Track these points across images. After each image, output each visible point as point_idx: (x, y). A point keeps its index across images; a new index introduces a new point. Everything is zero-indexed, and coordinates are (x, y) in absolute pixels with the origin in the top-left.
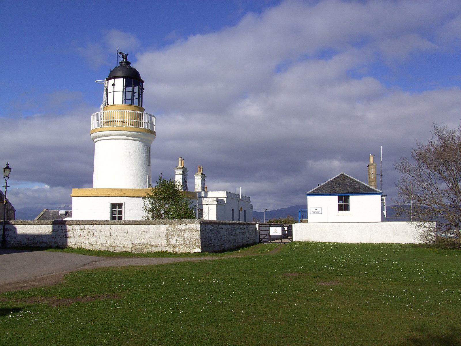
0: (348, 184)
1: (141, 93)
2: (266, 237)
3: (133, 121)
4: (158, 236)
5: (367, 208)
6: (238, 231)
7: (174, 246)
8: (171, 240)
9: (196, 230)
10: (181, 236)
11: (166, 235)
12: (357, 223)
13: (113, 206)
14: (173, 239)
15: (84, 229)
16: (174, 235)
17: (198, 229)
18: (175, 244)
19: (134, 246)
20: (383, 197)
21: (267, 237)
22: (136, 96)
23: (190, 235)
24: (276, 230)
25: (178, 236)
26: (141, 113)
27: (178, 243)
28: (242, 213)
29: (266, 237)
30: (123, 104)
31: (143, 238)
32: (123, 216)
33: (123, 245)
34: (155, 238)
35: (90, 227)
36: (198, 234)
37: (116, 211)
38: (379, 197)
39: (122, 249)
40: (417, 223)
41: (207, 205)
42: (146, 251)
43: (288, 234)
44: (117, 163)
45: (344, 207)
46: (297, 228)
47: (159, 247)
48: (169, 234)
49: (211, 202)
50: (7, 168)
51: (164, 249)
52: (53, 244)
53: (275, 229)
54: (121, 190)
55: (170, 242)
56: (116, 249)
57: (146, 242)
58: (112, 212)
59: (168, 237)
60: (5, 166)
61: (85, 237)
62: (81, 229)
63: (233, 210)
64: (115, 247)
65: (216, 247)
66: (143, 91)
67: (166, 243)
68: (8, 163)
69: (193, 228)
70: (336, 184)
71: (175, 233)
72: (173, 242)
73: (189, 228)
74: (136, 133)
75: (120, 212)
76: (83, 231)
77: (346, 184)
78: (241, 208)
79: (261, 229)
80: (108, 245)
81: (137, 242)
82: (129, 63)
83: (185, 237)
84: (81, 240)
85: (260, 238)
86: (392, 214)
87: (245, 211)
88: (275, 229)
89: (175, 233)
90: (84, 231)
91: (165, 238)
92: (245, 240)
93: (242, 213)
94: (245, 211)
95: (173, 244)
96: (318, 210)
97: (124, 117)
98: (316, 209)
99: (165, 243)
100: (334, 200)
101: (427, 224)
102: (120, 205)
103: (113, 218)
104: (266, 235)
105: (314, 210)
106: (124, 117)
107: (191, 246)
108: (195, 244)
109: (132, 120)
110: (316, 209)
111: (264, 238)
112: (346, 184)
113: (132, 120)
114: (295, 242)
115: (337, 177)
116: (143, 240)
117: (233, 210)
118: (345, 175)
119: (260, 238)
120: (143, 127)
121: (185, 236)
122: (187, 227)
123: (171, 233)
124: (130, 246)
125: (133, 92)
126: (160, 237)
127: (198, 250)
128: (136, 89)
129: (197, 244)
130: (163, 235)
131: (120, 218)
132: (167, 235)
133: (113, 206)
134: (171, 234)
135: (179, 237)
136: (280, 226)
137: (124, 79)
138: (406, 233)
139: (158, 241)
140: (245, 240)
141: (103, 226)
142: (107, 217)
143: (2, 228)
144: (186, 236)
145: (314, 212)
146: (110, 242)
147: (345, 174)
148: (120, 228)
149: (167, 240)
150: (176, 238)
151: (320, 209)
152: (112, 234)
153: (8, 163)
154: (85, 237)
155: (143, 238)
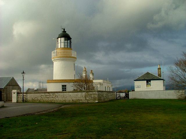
1: (70, 42)
6: (109, 94)
7: (88, 100)
12: (156, 90)
13: (63, 86)
20: (164, 81)
22: (69, 44)
28: (109, 88)
32: (67, 90)
35: (56, 94)
37: (64, 88)
38: (54, 79)
42: (78, 102)
43: (127, 95)
46: (130, 93)
51: (84, 101)
52: (106, 100)
54: (62, 80)
56: (66, 102)
58: (63, 88)
72: (87, 98)
75: (65, 88)
79: (117, 94)
81: (74, 99)
84: (52, 99)
86: (168, 87)
93: (109, 88)
99: (84, 99)
101: (181, 91)
102: (65, 86)
103: (63, 90)
111: (118, 97)
119: (116, 97)
121: (92, 96)
124: (71, 100)
128: (69, 41)
131: (65, 90)
133: (63, 86)
136: (29, 97)
138: (172, 95)
139: (82, 98)
141: (61, 93)
142: (61, 90)
143: (22, 95)
146: (64, 99)
149: (85, 98)
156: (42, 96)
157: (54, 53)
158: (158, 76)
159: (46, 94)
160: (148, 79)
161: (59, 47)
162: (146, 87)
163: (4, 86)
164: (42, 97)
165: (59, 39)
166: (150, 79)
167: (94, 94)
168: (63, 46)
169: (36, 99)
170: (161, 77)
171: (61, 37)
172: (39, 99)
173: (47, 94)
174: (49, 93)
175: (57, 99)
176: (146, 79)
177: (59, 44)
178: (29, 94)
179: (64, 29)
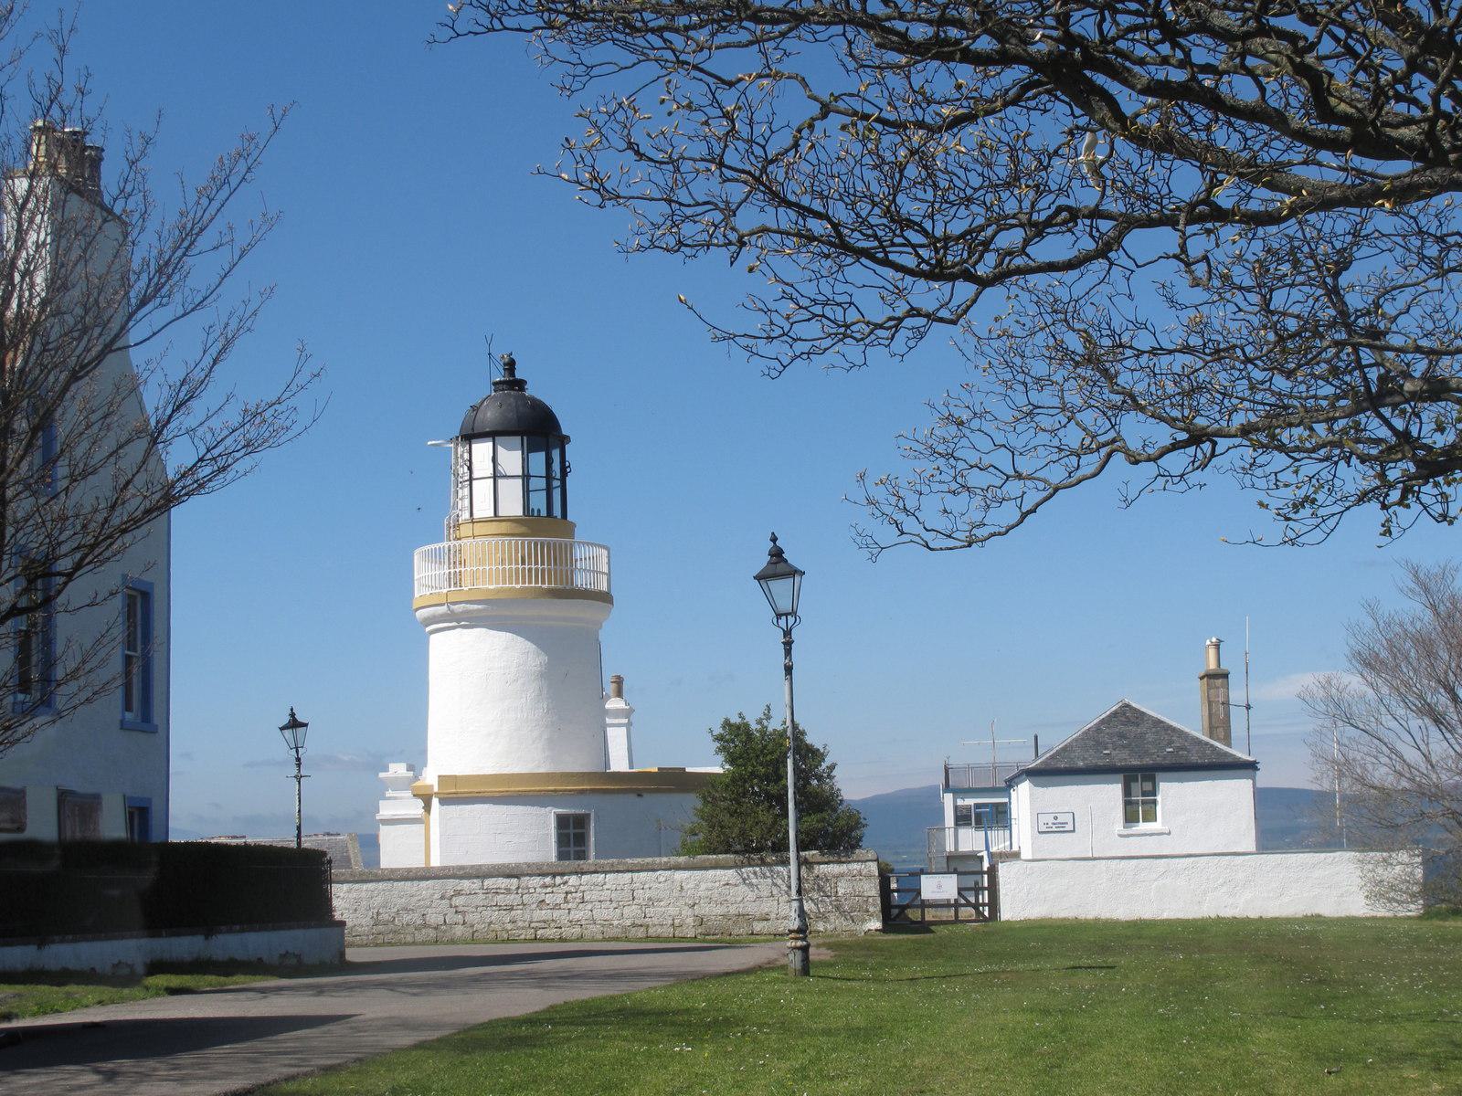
0: (1150, 737)
3: (517, 569)
5: (1204, 813)
9: (869, 876)
12: (1198, 861)
15: (555, 885)
19: (701, 921)
26: (523, 543)
33: (670, 922)
39: (668, 932)
40: (1378, 855)
44: (476, 702)
45: (1137, 809)
50: (294, 724)
54: (583, 774)
58: (562, 840)
60: (286, 720)
61: (557, 907)
62: (545, 886)
64: (648, 926)
68: (292, 710)
70: (1111, 736)
74: (476, 607)
76: (549, 890)
77: (1142, 736)
80: (628, 923)
81: (712, 911)
82: (520, 385)
90: (555, 889)
97: (490, 559)
98: (1056, 818)
100: (1110, 794)
105: (1050, 819)
106: (490, 559)
109: (527, 567)
110: (1056, 818)
112: (1142, 736)
113: (527, 567)
114: (1012, 927)
115: (1109, 716)
118: (1135, 709)
124: (690, 921)
127: (875, 924)
129: (871, 909)
133: (562, 821)
137: (525, 438)
138: (1332, 887)
144: (843, 891)
146: (631, 912)
147: (1134, 705)
148: (662, 879)
152: (638, 893)
153: (292, 710)
154: (557, 907)
156: (458, 893)
157: (436, 558)
158: (1206, 739)
159: (489, 882)
160: (1136, 759)
161: (484, 509)
162: (1119, 825)
163: (1152, 710)
164: (458, 901)
165: (482, 450)
166: (1147, 761)
167: (853, 876)
168: (512, 505)
169: (406, 918)
170: (1227, 740)
171: (492, 435)
172: (434, 918)
173: (500, 880)
174: (962, 922)
175: (576, 915)
176: (1122, 757)
177: (483, 489)
178: (345, 887)
179: (510, 366)
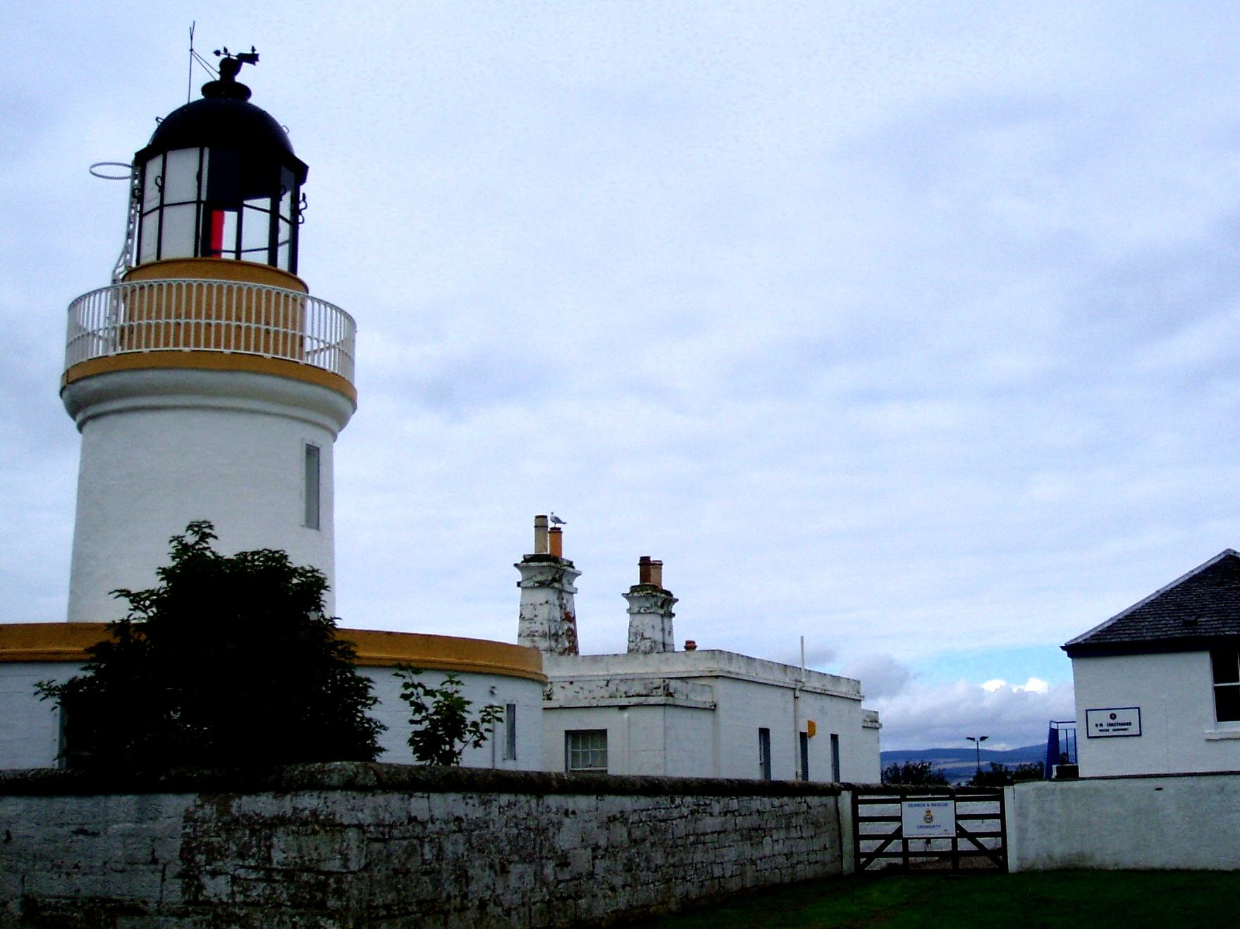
2: (889, 848)
4: (143, 854)
8: (206, 880)
10: (253, 856)
11: (182, 852)
14: (214, 874)
16: (220, 853)
17: (337, 816)
18: (225, 899)
21: (895, 846)
23: (300, 850)
24: (928, 818)
25: (241, 855)
27: (240, 898)
29: (889, 848)
30: (196, 254)
31: (76, 866)
34: (128, 867)
36: (337, 847)
41: (623, 708)
47: (147, 919)
48: (198, 847)
49: (639, 695)
53: (926, 808)
55: (201, 888)
57: (87, 885)
59: (192, 860)
63: (764, 733)
65: (508, 914)
66: (302, 205)
67: (184, 893)
69: (314, 813)
71: (227, 841)
72: (216, 888)
73: (295, 809)
78: (811, 725)
79: (864, 810)
83: (275, 865)
85: (857, 854)
87: (834, 738)
88: (926, 808)
89: (227, 841)
91: (178, 866)
92: (760, 865)
94: (834, 738)
95: (215, 900)
96: (1122, 717)
98: (1113, 716)
104: (888, 839)
105: (1105, 718)
107: (301, 915)
108: (322, 905)
110: (1113, 716)
111: (879, 853)
116: (78, 880)
117: (764, 733)
119: (857, 854)
120: (276, 352)
121: (277, 856)
122: (287, 805)
123: (205, 840)
125: (274, 214)
126: (154, 861)
130: (171, 851)
132: (187, 853)
134: (207, 844)
135: (247, 863)
137: (207, 151)
140: (760, 865)
145: (1105, 727)
149: (190, 877)
150: (229, 865)
151: (1131, 716)
155: (76, 866)
